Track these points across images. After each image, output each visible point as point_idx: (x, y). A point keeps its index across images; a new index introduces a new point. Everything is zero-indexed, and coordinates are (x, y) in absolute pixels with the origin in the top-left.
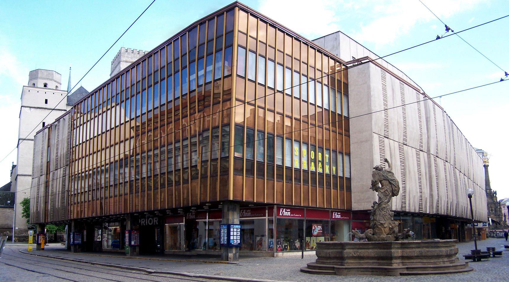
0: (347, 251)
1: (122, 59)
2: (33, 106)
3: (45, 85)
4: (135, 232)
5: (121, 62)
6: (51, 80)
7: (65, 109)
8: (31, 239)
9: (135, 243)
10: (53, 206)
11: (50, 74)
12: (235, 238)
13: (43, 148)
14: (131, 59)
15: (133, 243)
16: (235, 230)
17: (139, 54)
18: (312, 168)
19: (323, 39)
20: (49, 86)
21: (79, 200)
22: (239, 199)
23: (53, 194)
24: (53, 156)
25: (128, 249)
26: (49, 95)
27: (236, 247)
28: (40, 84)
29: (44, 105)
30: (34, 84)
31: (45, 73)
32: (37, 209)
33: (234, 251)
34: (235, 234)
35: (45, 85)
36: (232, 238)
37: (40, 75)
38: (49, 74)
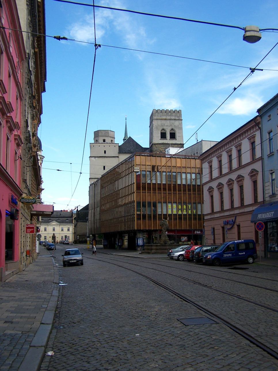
0: (145, 247)
1: (154, 118)
2: (97, 156)
3: (104, 141)
4: (121, 240)
5: (153, 120)
6: (108, 136)
7: (118, 156)
8: (88, 242)
9: (121, 244)
10: (96, 226)
11: (106, 133)
12: (140, 243)
13: (92, 194)
14: (161, 117)
15: (119, 244)
16: (140, 240)
17: (166, 112)
18: (180, 212)
19: (210, 142)
20: (106, 141)
21: (127, 215)
22: (139, 229)
23: (96, 220)
24: (96, 201)
25: (116, 246)
26: (107, 147)
27: (141, 246)
28: (101, 141)
29: (104, 155)
30: (97, 140)
31: (104, 133)
32: (91, 227)
33: (140, 248)
34: (140, 241)
35: (104, 141)
36: (139, 243)
37: (100, 134)
38: (106, 133)
